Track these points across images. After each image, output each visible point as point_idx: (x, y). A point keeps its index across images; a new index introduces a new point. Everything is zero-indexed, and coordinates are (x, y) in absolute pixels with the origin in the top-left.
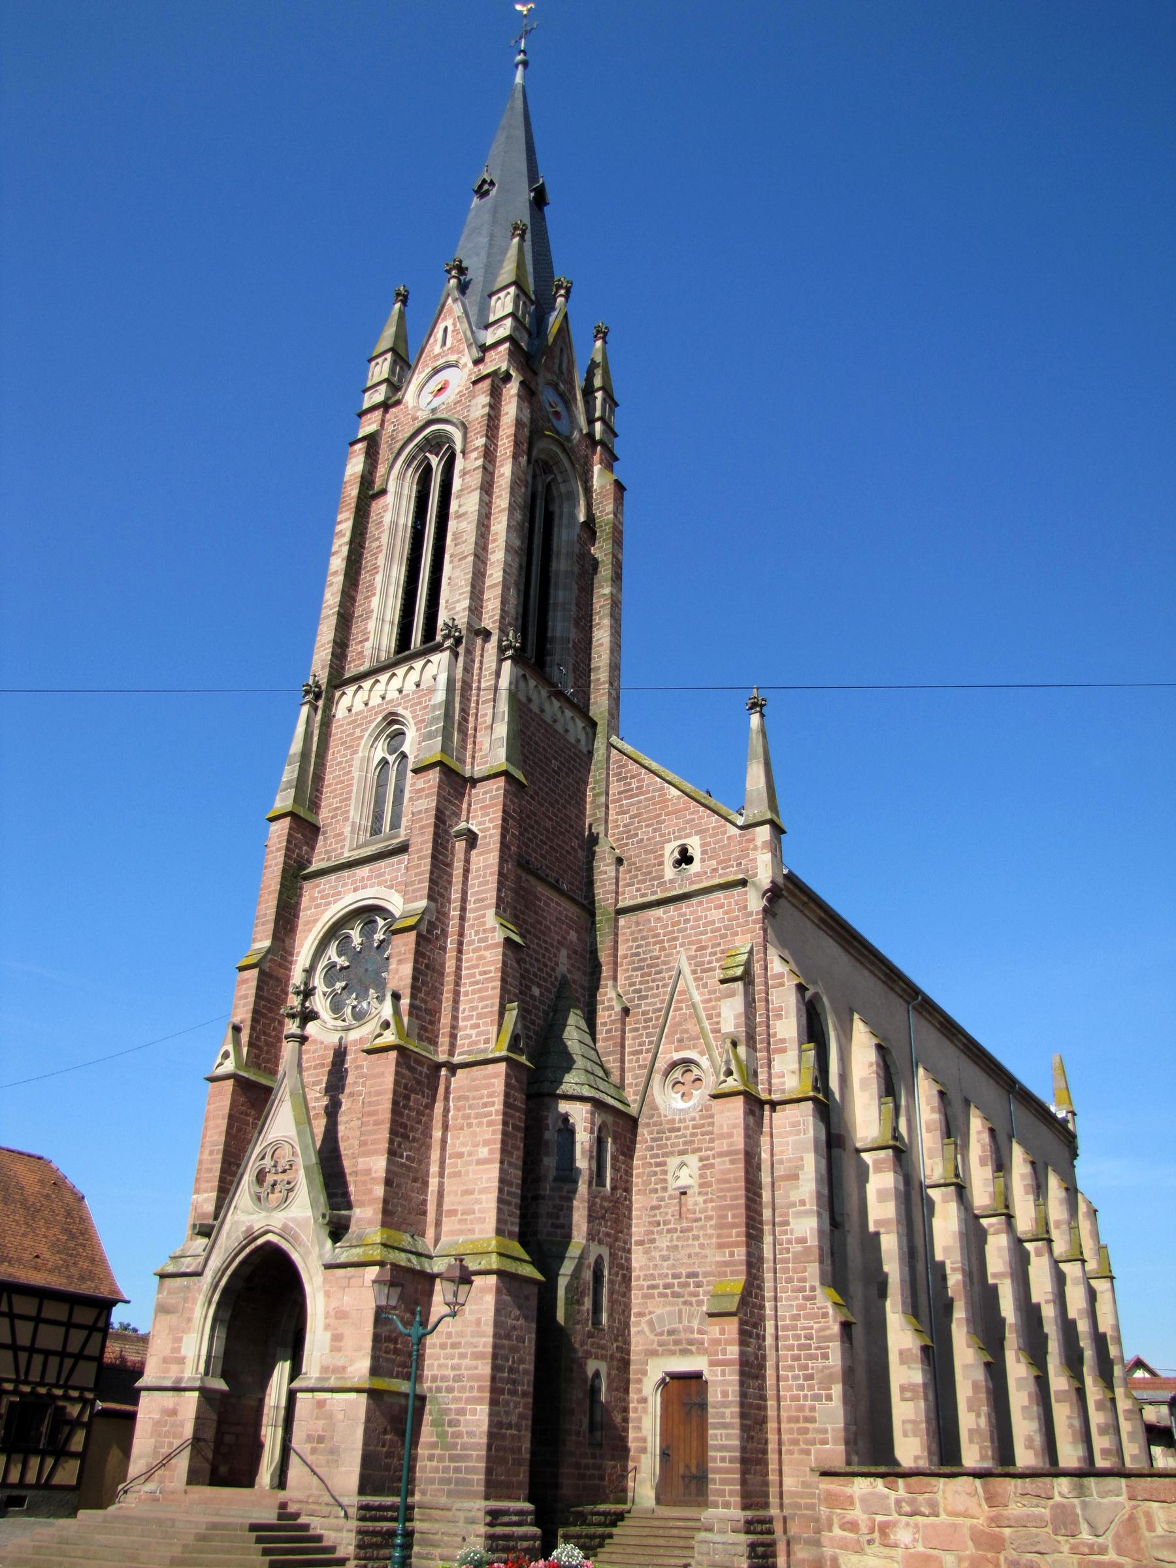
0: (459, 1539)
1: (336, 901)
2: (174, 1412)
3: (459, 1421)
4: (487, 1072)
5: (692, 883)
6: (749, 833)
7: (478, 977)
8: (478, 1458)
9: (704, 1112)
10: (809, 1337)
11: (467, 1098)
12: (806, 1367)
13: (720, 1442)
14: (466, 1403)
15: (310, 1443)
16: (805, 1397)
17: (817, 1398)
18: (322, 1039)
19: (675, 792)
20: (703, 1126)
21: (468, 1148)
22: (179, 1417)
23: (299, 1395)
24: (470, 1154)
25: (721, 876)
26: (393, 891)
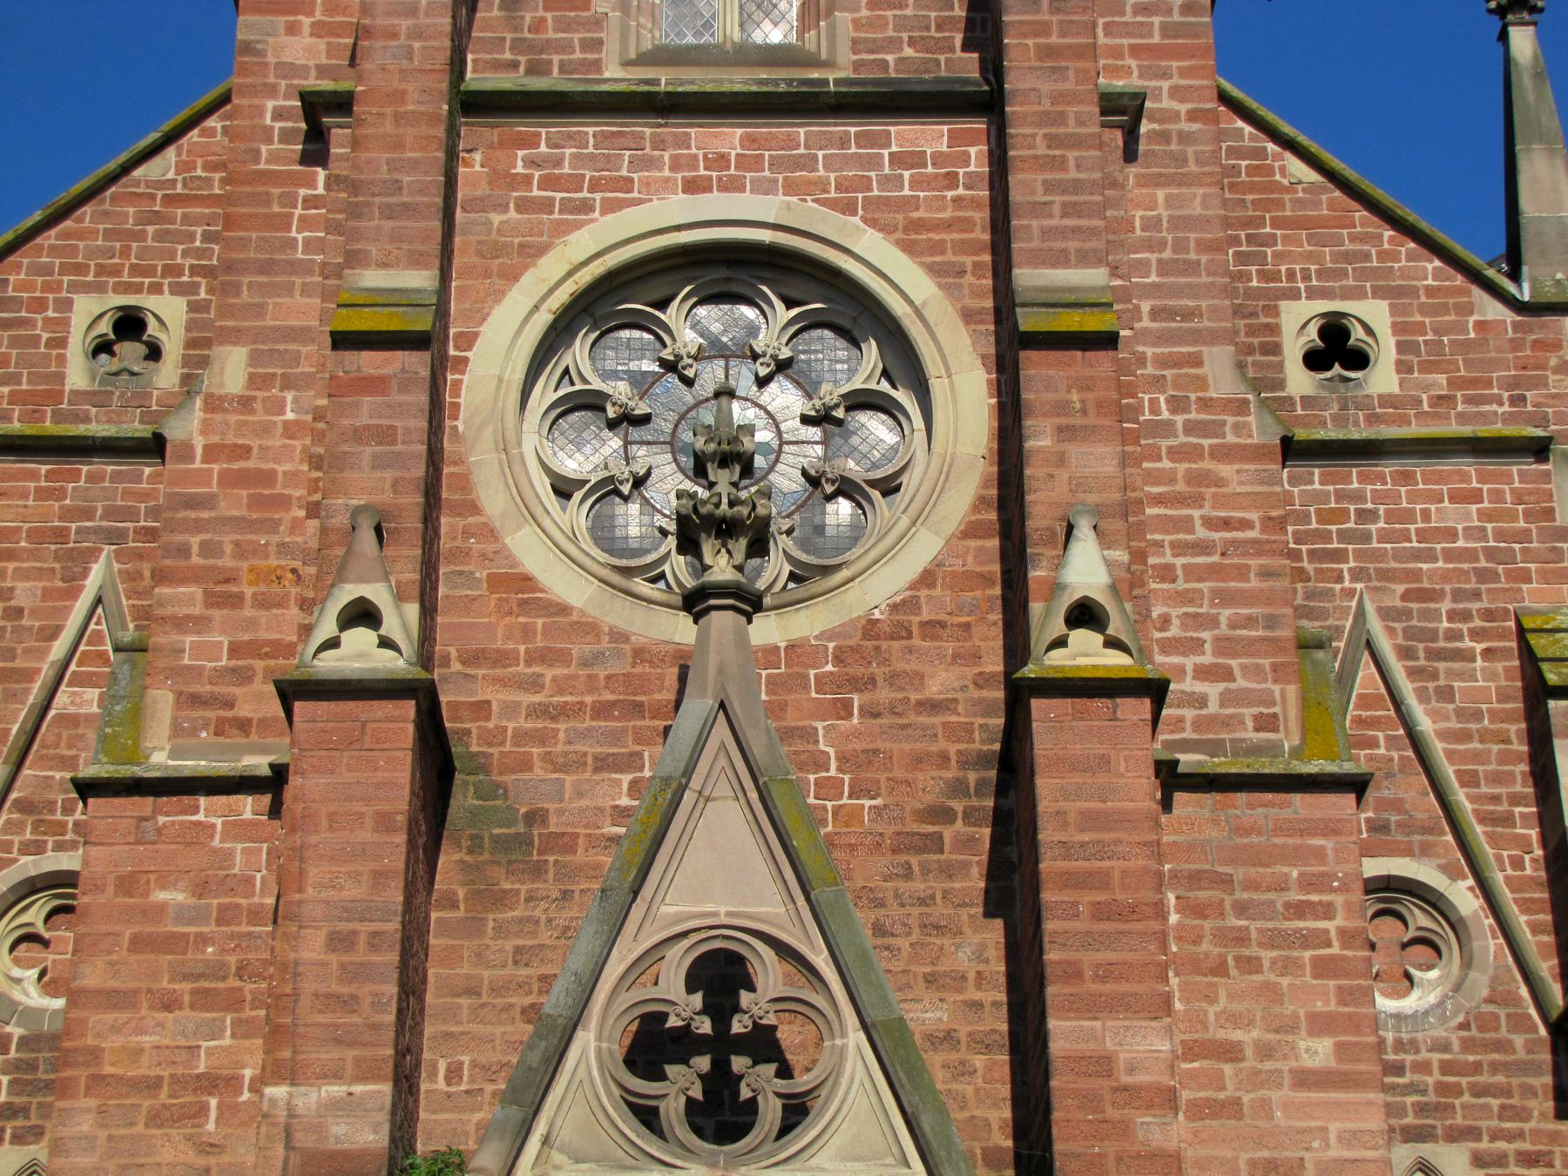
1: (610, 207)
4: (1287, 813)
5: (1373, 419)
6: (1543, 326)
7: (1201, 533)
9: (1474, 1032)
11: (1225, 882)
18: (621, 624)
19: (1298, 169)
20: (1476, 1068)
21: (1255, 1034)
25: (1463, 418)
26: (856, 220)
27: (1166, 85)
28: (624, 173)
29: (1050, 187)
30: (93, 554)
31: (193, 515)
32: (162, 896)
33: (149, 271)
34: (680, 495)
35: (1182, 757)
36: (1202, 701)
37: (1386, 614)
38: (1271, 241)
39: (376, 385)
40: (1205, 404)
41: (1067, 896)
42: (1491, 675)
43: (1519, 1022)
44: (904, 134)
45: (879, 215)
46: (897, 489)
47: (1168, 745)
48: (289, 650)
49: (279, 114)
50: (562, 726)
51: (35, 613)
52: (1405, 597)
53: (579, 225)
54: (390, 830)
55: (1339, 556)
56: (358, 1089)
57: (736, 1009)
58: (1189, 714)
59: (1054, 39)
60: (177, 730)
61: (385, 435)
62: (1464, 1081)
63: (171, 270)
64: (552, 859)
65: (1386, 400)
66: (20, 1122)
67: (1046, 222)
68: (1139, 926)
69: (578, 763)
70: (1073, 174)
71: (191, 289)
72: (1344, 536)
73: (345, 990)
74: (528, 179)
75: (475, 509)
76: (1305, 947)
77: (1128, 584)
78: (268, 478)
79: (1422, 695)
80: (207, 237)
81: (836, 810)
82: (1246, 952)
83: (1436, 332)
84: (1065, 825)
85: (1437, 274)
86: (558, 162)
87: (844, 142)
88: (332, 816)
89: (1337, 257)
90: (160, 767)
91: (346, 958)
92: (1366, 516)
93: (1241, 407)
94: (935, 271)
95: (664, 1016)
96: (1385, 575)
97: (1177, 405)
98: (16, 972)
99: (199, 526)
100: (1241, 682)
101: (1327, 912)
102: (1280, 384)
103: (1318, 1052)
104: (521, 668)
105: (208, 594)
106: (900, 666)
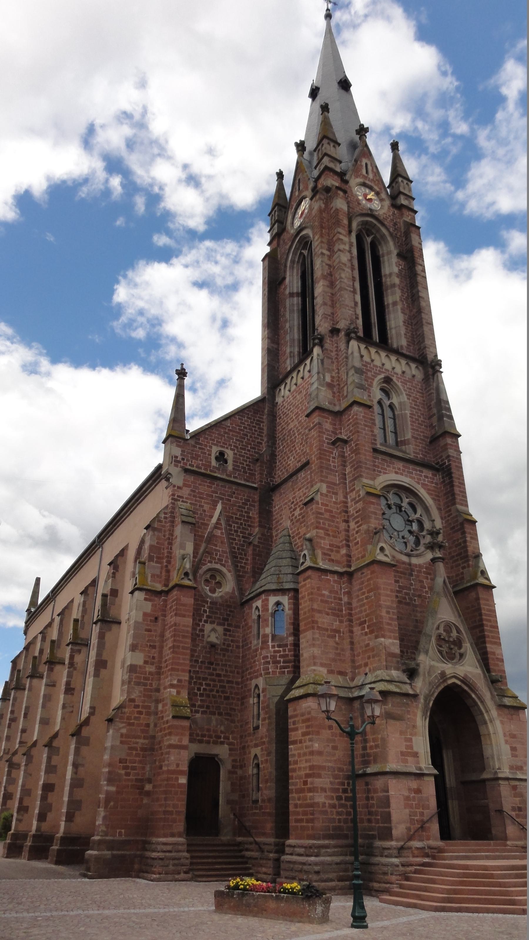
2: (418, 791)
22: (424, 795)
32: (324, 592)
33: (226, 444)
45: (424, 485)
60: (322, 560)
63: (230, 445)
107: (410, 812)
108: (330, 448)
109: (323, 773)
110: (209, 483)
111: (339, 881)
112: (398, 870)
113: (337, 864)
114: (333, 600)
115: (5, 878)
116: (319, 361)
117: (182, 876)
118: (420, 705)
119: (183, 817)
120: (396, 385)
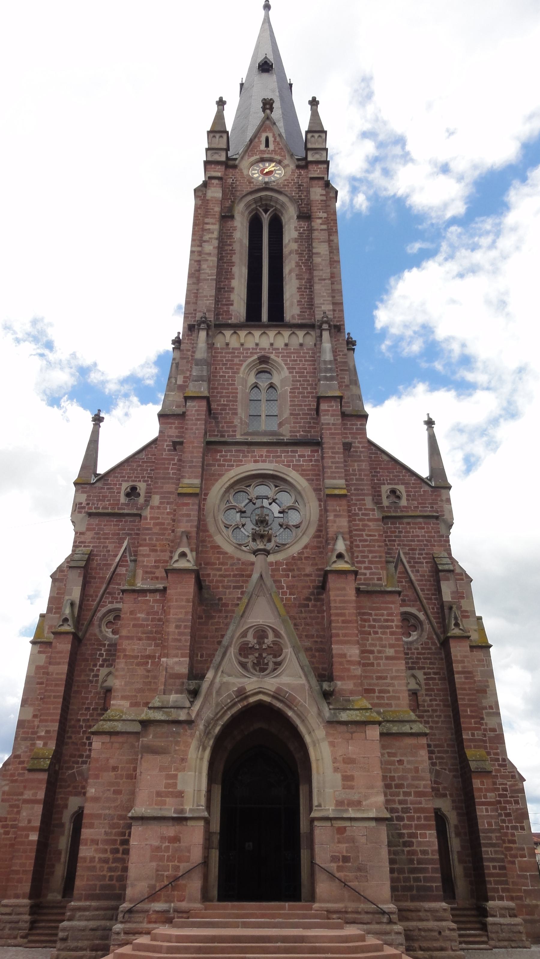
0: (436, 934)
1: (238, 466)
3: (413, 843)
5: (402, 511)
7: (365, 537)
8: (434, 870)
9: (424, 646)
10: (505, 790)
11: (370, 614)
12: (505, 808)
13: (491, 856)
14: (416, 829)
15: (335, 862)
16: (507, 827)
17: (515, 828)
20: (424, 654)
23: (316, 823)
24: (379, 652)
25: (421, 511)
27: (357, 441)
28: (241, 458)
29: (332, 463)
30: (125, 539)
31: (147, 532)
32: (139, 615)
33: (139, 477)
34: (253, 529)
35: (360, 586)
36: (365, 574)
37: (405, 554)
38: (379, 472)
39: (187, 504)
40: (366, 509)
41: (336, 618)
42: (427, 567)
43: (434, 643)
44: (301, 450)
45: (296, 468)
46: (299, 527)
47: (359, 584)
48: (167, 562)
49: (167, 446)
50: (226, 579)
51: (112, 551)
52: (409, 550)
53: (230, 470)
54: (189, 602)
55: (394, 541)
56: (181, 659)
57: (264, 643)
58: (362, 577)
59: (333, 431)
60: (143, 579)
61: (188, 515)
62: (422, 656)
64: (223, 609)
65: (404, 507)
66: (108, 663)
67: (331, 470)
68: (351, 625)
69: (229, 587)
70: (337, 460)
71: (147, 481)
72: (396, 536)
73: (179, 637)
74: (220, 460)
75: (208, 531)
76: (388, 629)
77: (350, 549)
78: (163, 524)
79: (412, 571)
80: (151, 470)
81: (286, 598)
82: (375, 630)
83: (414, 492)
84: (336, 602)
85: (415, 480)
86: (227, 456)
87: (288, 452)
88: (176, 599)
89: (393, 476)
90: (139, 586)
91: (179, 630)
92: (400, 532)
93: (373, 510)
94: (308, 480)
95: (248, 644)
96: (404, 545)
97: (360, 509)
98: (107, 630)
99: (148, 534)
100: (374, 570)
101: (392, 621)
102: (382, 503)
103: (390, 652)
104: (217, 566)
105: (150, 549)
106: (300, 566)
107: (158, 865)
108: (171, 455)
109: (96, 822)
110: (116, 521)
111: (92, 950)
112: (118, 939)
113: (92, 930)
114: (149, 623)
115: (82, 940)
116: (174, 364)
117: (19, 940)
118: (197, 733)
119: (30, 876)
120: (275, 361)
